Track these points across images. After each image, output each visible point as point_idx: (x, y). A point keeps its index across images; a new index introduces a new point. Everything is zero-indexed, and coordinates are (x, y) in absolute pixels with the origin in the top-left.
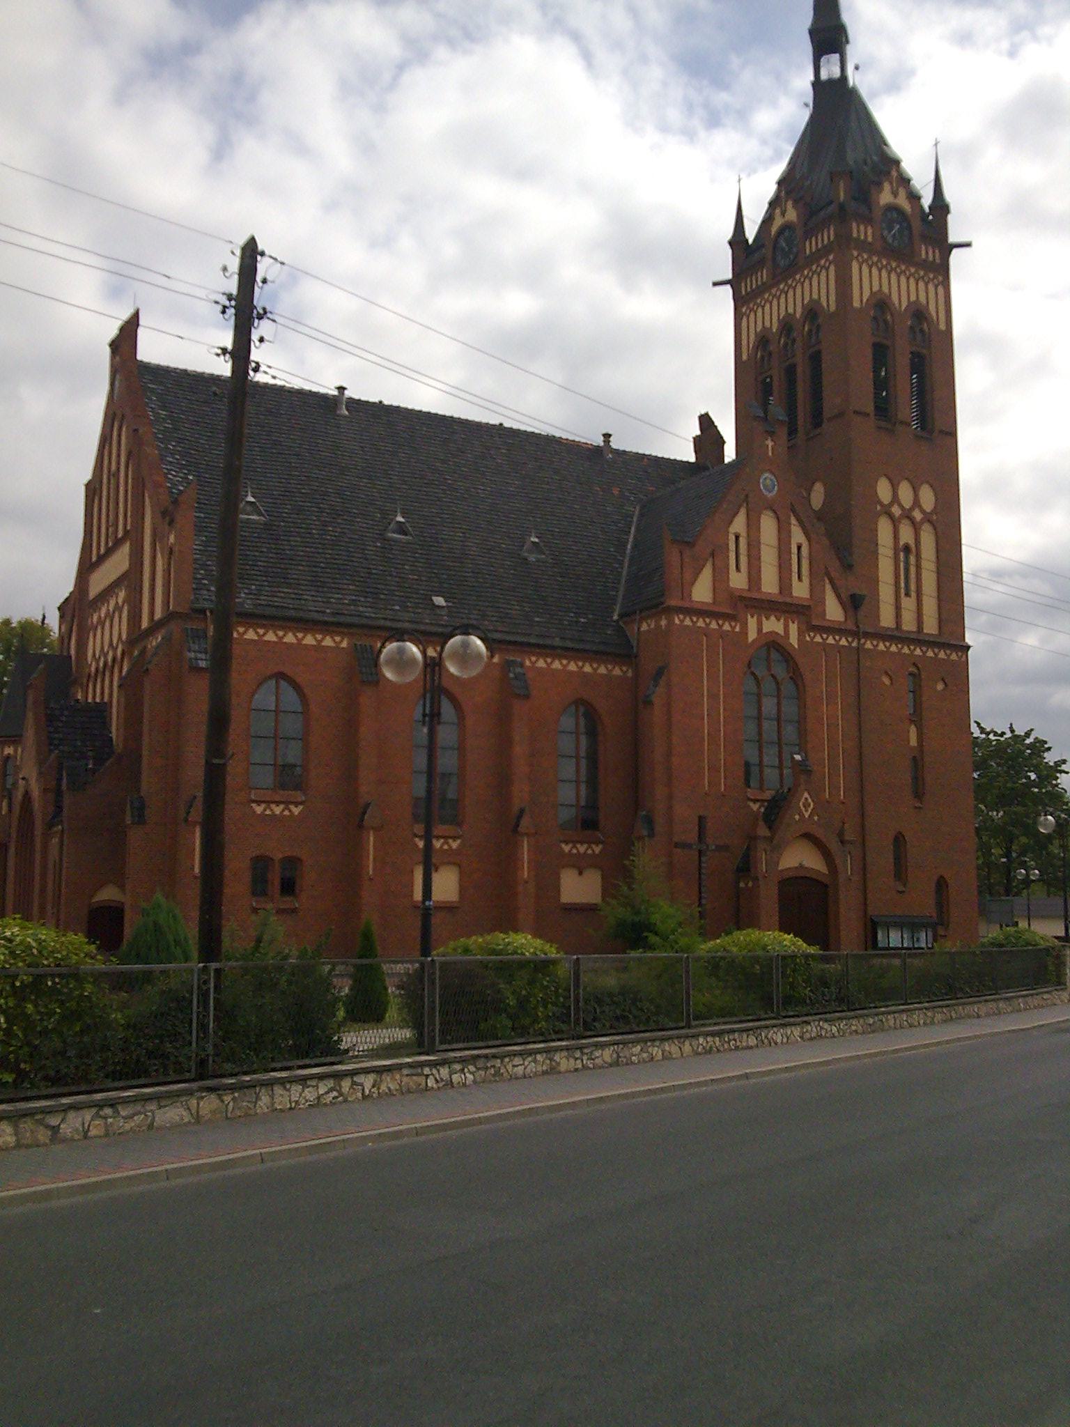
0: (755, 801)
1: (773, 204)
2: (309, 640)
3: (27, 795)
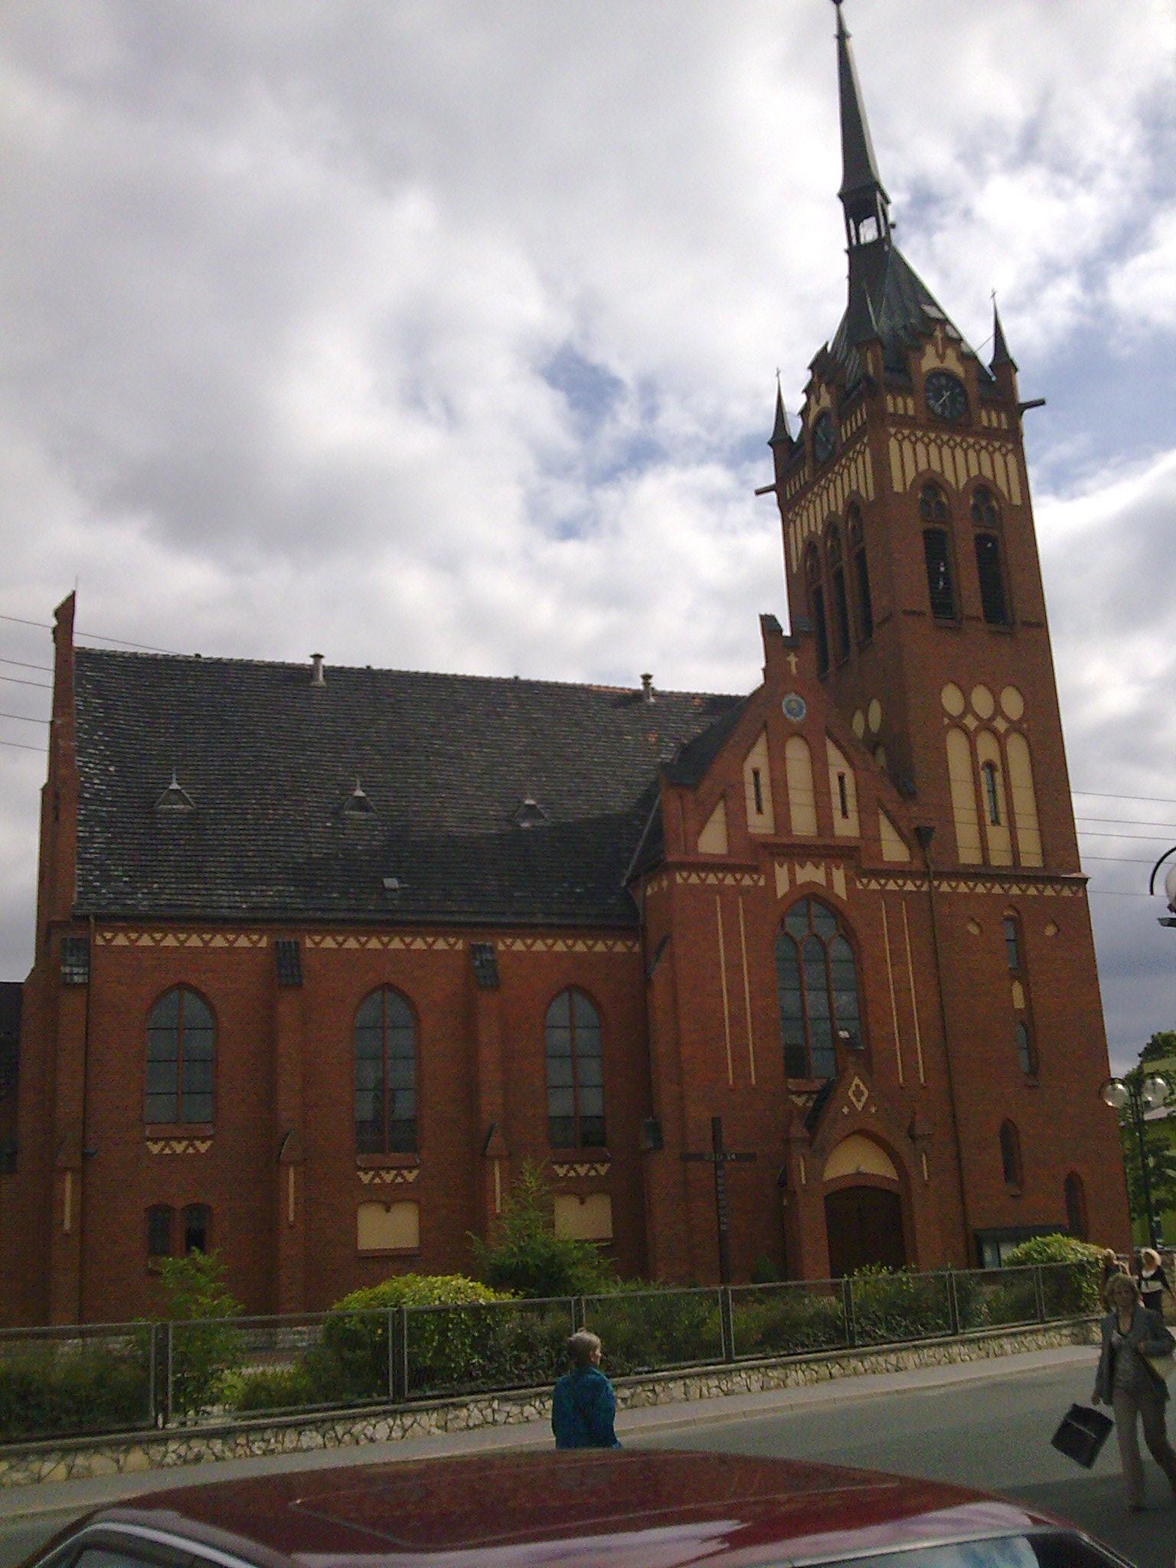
0: (799, 1094)
2: (219, 941)
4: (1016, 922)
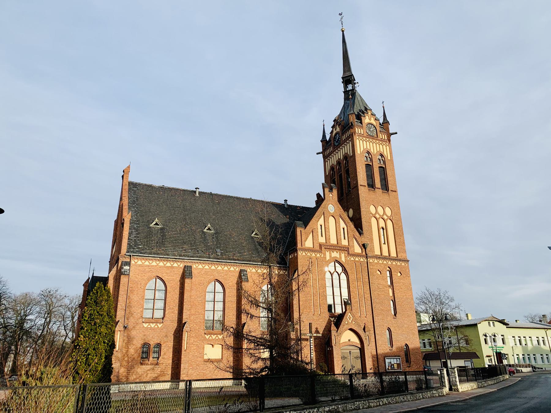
1: (333, 127)
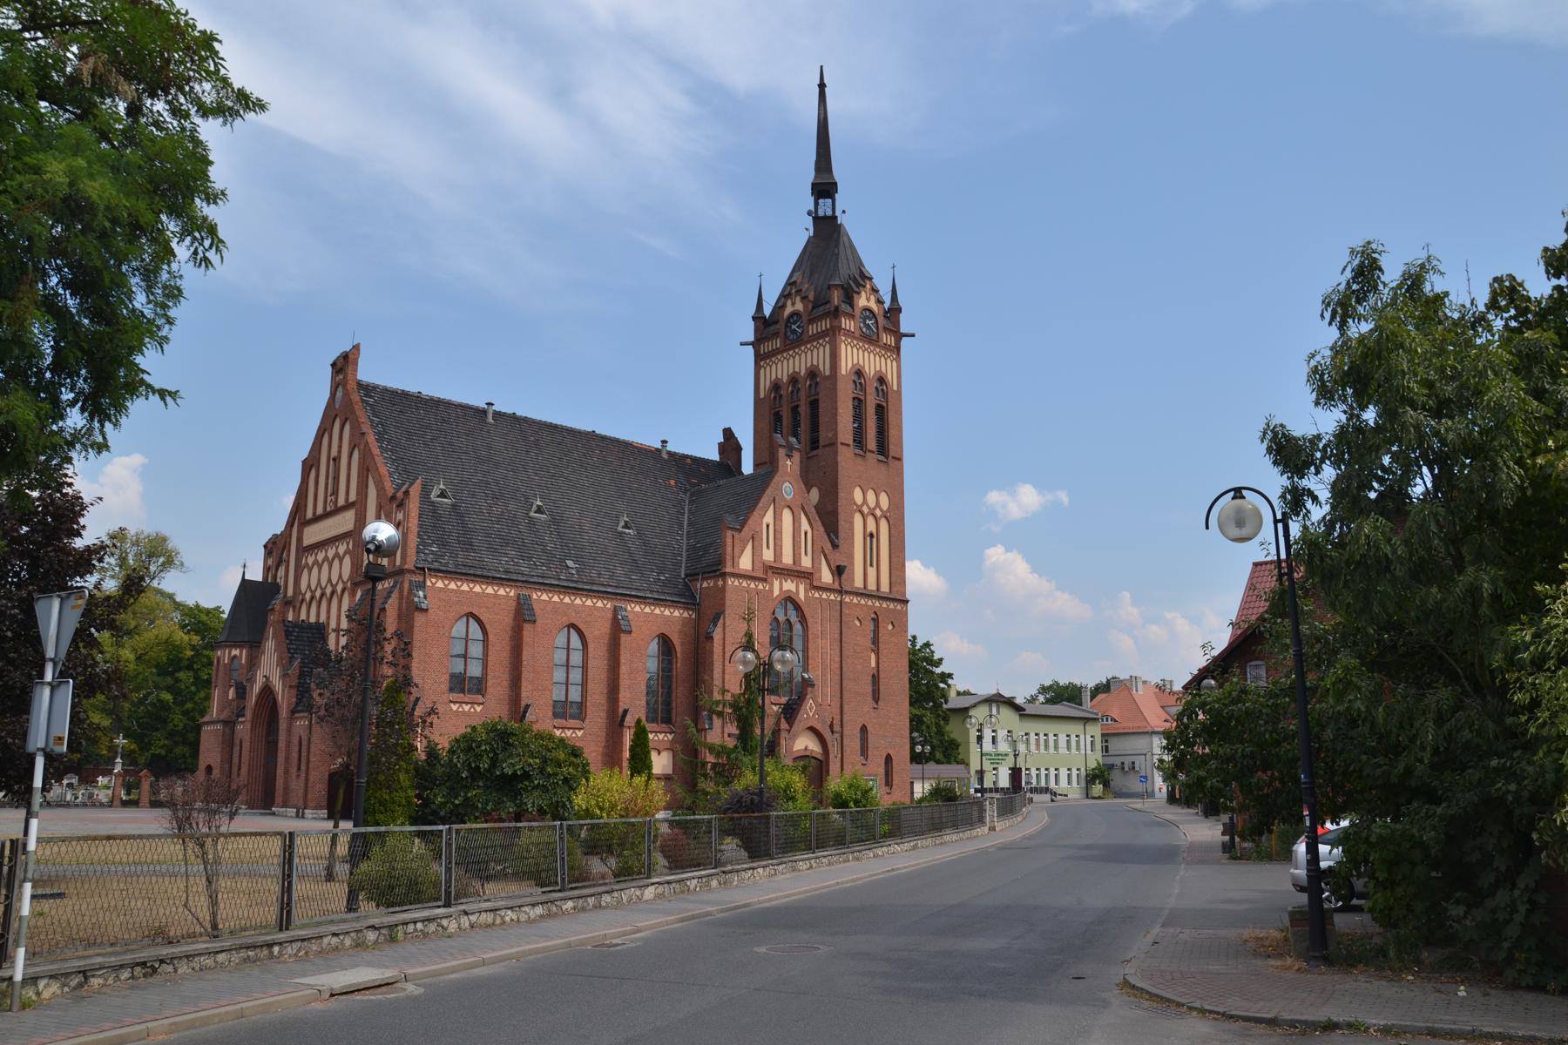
2: (490, 590)
3: (267, 690)
4: (876, 621)
